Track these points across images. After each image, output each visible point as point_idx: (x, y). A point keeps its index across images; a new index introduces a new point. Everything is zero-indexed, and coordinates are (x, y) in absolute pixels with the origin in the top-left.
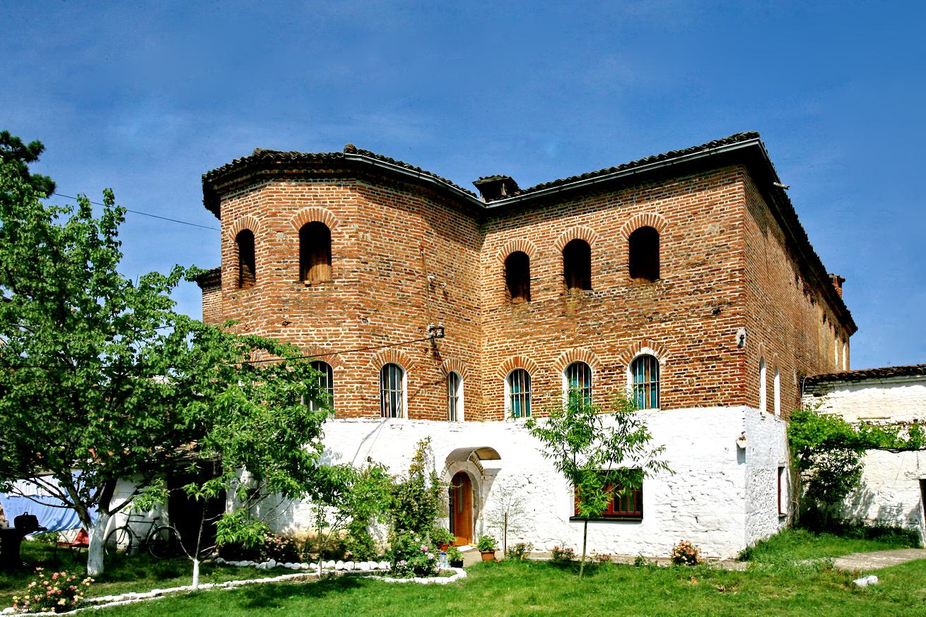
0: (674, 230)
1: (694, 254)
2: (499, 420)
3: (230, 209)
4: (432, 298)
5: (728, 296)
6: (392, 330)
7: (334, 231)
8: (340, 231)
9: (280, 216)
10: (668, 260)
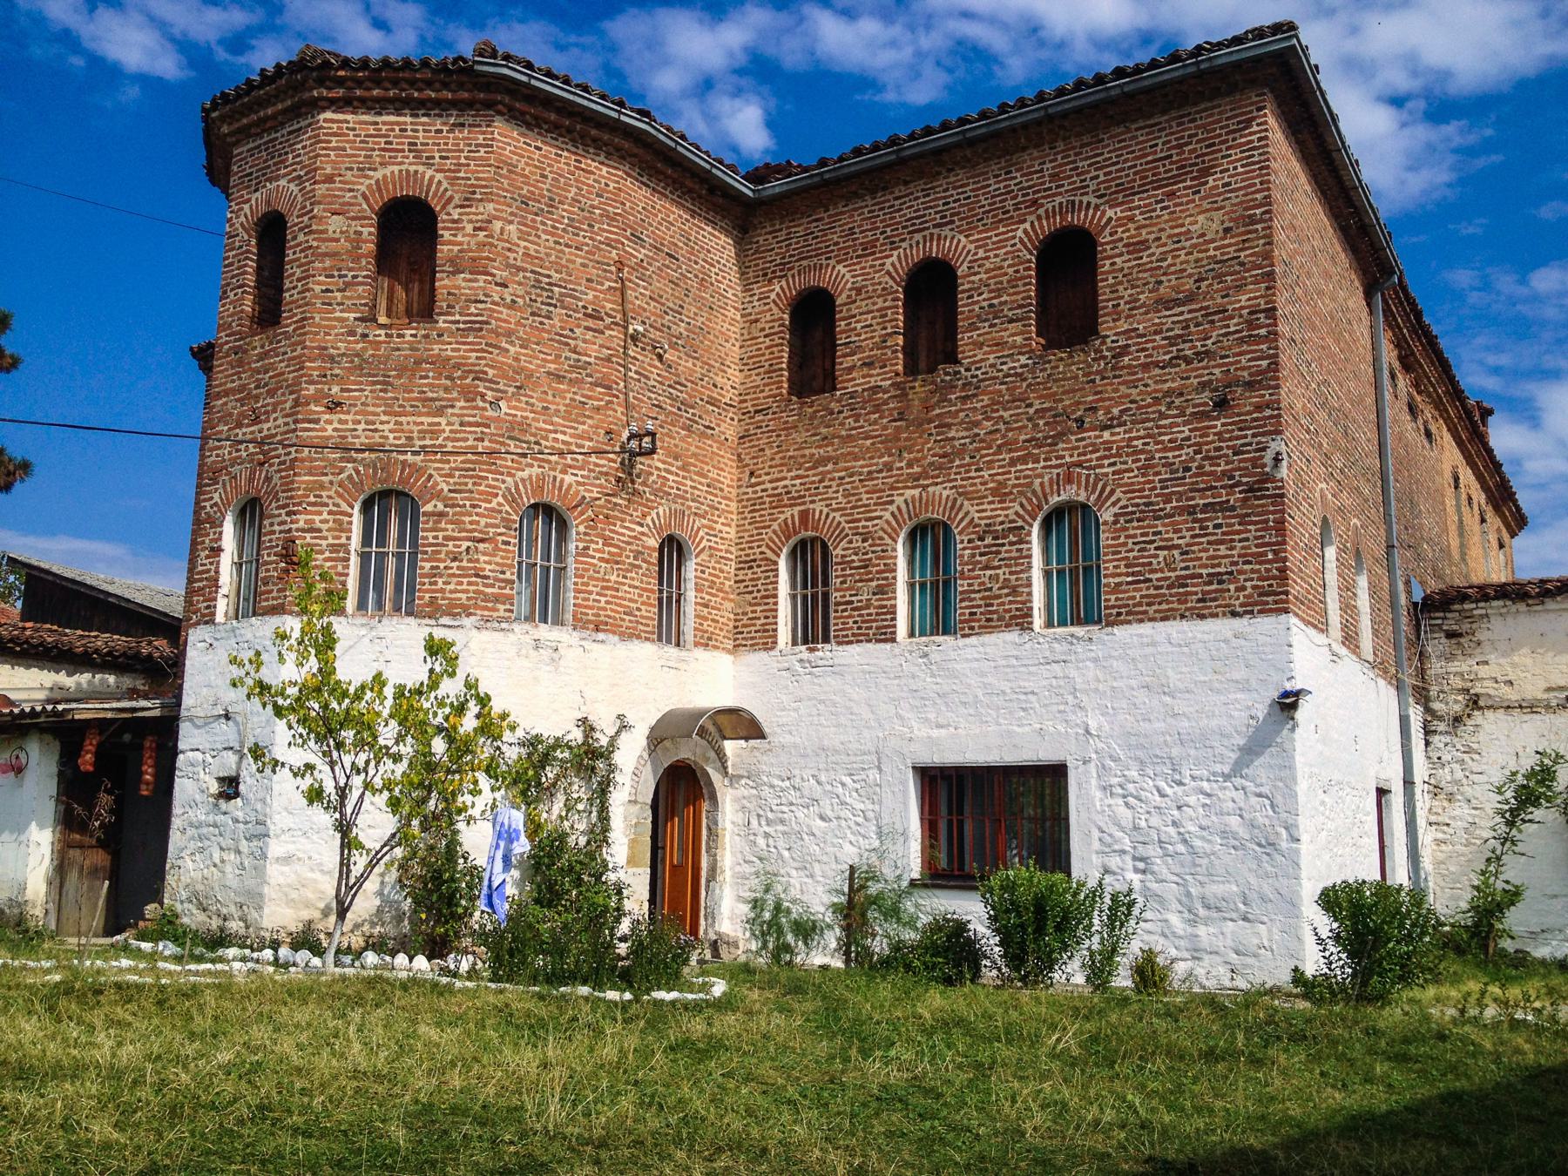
0: (1128, 230)
1: (1170, 281)
3: (248, 171)
4: (636, 372)
5: (1243, 369)
6: (551, 431)
7: (445, 217)
8: (456, 217)
9: (340, 182)
10: (1115, 295)
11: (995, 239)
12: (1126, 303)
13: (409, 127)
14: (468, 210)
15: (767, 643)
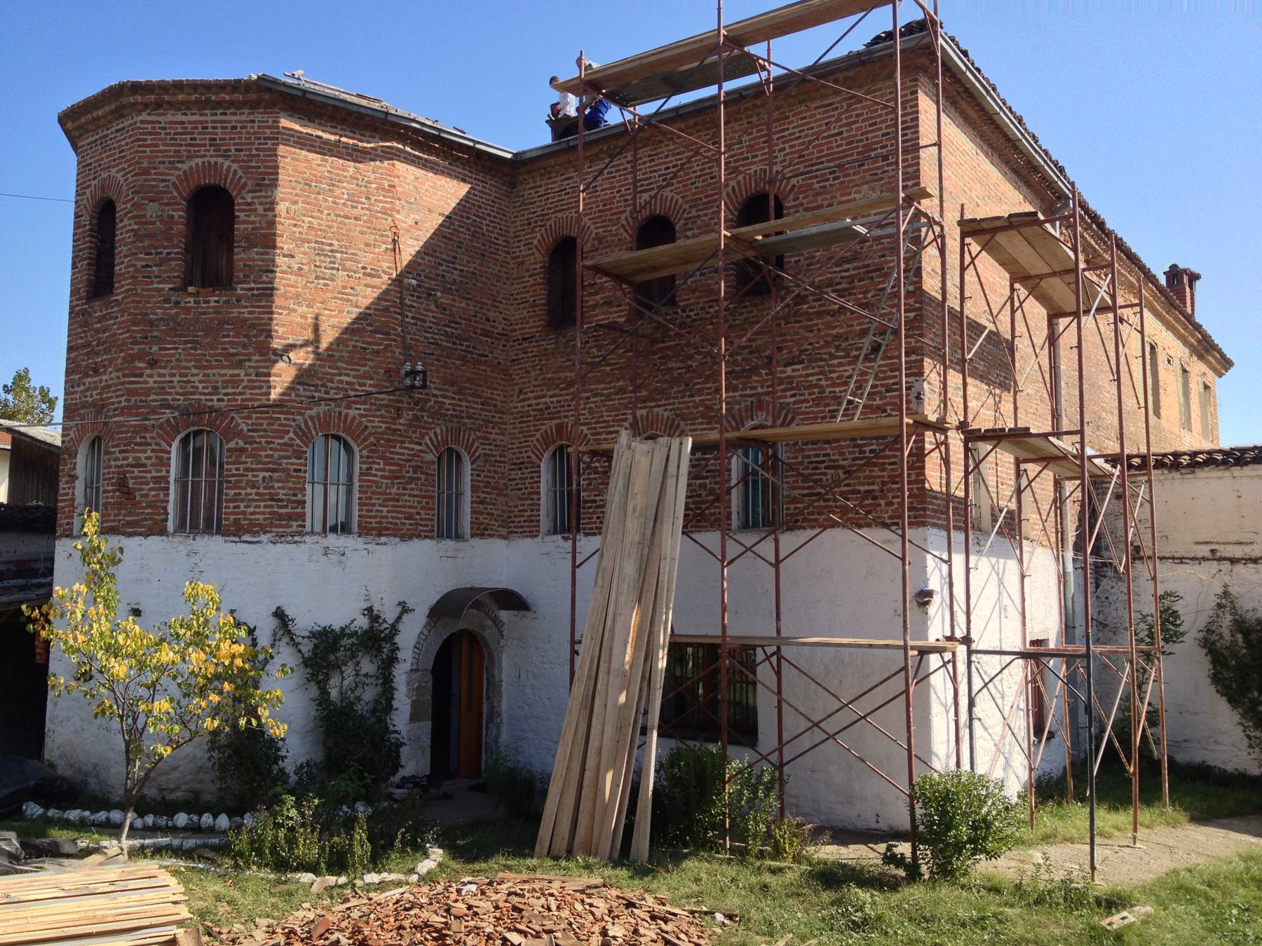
2: (531, 537)
3: (89, 161)
4: (412, 318)
7: (240, 201)
8: (249, 200)
9: (155, 174)
11: (704, 200)
12: (805, 259)
13: (210, 125)
14: (258, 194)
15: (532, 532)
